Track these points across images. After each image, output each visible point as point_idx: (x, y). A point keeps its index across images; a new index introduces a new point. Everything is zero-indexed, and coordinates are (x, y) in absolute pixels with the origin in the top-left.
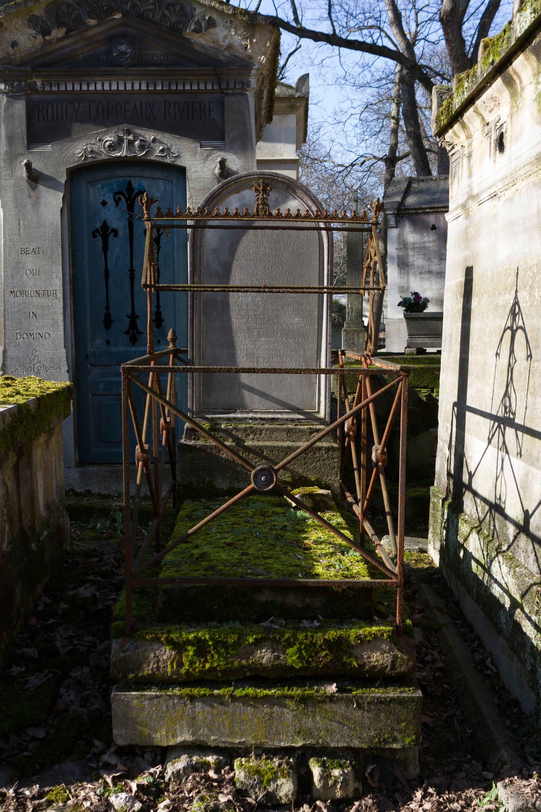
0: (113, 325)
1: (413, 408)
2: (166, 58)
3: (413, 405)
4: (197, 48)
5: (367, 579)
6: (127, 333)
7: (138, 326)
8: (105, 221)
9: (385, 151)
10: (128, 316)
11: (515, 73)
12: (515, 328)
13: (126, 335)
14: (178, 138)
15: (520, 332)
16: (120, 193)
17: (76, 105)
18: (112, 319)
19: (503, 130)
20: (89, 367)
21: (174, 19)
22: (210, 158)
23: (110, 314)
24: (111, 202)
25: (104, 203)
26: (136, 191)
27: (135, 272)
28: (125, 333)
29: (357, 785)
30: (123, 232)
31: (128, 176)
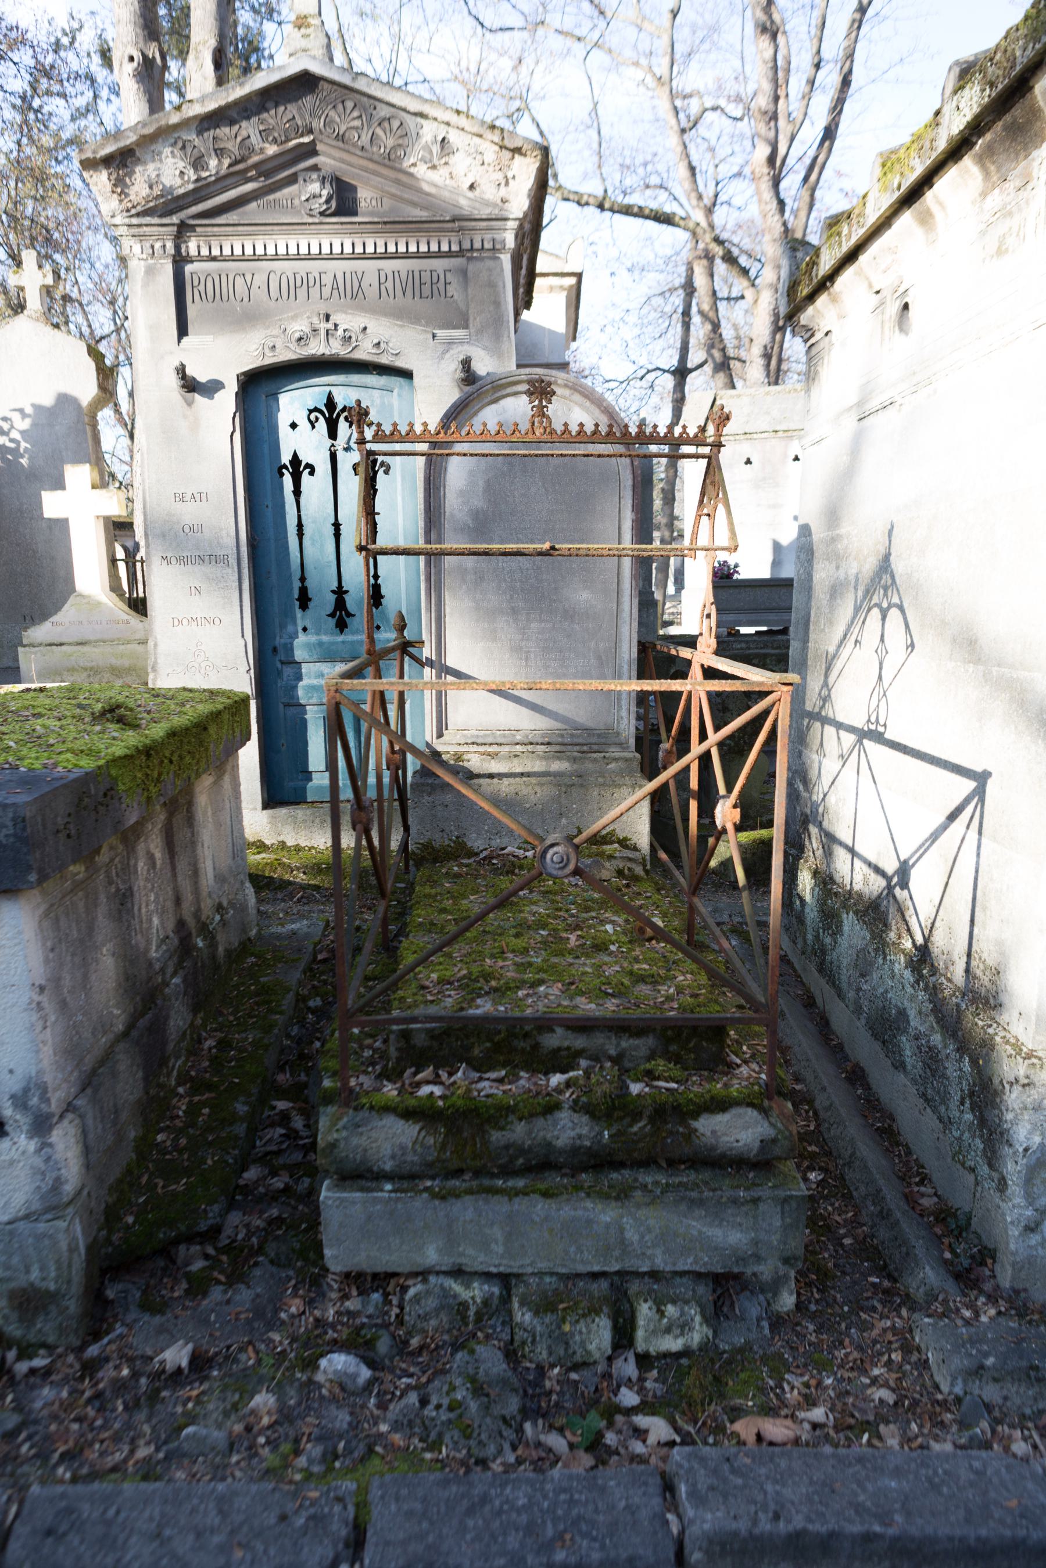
0: (311, 604)
4: (426, 188)
6: (332, 615)
9: (671, 360)
10: (333, 592)
11: (940, 204)
12: (885, 605)
14: (401, 326)
15: (894, 613)
16: (316, 410)
17: (249, 278)
19: (906, 300)
20: (279, 665)
21: (391, 142)
22: (448, 355)
25: (294, 426)
26: (339, 407)
30: (323, 467)
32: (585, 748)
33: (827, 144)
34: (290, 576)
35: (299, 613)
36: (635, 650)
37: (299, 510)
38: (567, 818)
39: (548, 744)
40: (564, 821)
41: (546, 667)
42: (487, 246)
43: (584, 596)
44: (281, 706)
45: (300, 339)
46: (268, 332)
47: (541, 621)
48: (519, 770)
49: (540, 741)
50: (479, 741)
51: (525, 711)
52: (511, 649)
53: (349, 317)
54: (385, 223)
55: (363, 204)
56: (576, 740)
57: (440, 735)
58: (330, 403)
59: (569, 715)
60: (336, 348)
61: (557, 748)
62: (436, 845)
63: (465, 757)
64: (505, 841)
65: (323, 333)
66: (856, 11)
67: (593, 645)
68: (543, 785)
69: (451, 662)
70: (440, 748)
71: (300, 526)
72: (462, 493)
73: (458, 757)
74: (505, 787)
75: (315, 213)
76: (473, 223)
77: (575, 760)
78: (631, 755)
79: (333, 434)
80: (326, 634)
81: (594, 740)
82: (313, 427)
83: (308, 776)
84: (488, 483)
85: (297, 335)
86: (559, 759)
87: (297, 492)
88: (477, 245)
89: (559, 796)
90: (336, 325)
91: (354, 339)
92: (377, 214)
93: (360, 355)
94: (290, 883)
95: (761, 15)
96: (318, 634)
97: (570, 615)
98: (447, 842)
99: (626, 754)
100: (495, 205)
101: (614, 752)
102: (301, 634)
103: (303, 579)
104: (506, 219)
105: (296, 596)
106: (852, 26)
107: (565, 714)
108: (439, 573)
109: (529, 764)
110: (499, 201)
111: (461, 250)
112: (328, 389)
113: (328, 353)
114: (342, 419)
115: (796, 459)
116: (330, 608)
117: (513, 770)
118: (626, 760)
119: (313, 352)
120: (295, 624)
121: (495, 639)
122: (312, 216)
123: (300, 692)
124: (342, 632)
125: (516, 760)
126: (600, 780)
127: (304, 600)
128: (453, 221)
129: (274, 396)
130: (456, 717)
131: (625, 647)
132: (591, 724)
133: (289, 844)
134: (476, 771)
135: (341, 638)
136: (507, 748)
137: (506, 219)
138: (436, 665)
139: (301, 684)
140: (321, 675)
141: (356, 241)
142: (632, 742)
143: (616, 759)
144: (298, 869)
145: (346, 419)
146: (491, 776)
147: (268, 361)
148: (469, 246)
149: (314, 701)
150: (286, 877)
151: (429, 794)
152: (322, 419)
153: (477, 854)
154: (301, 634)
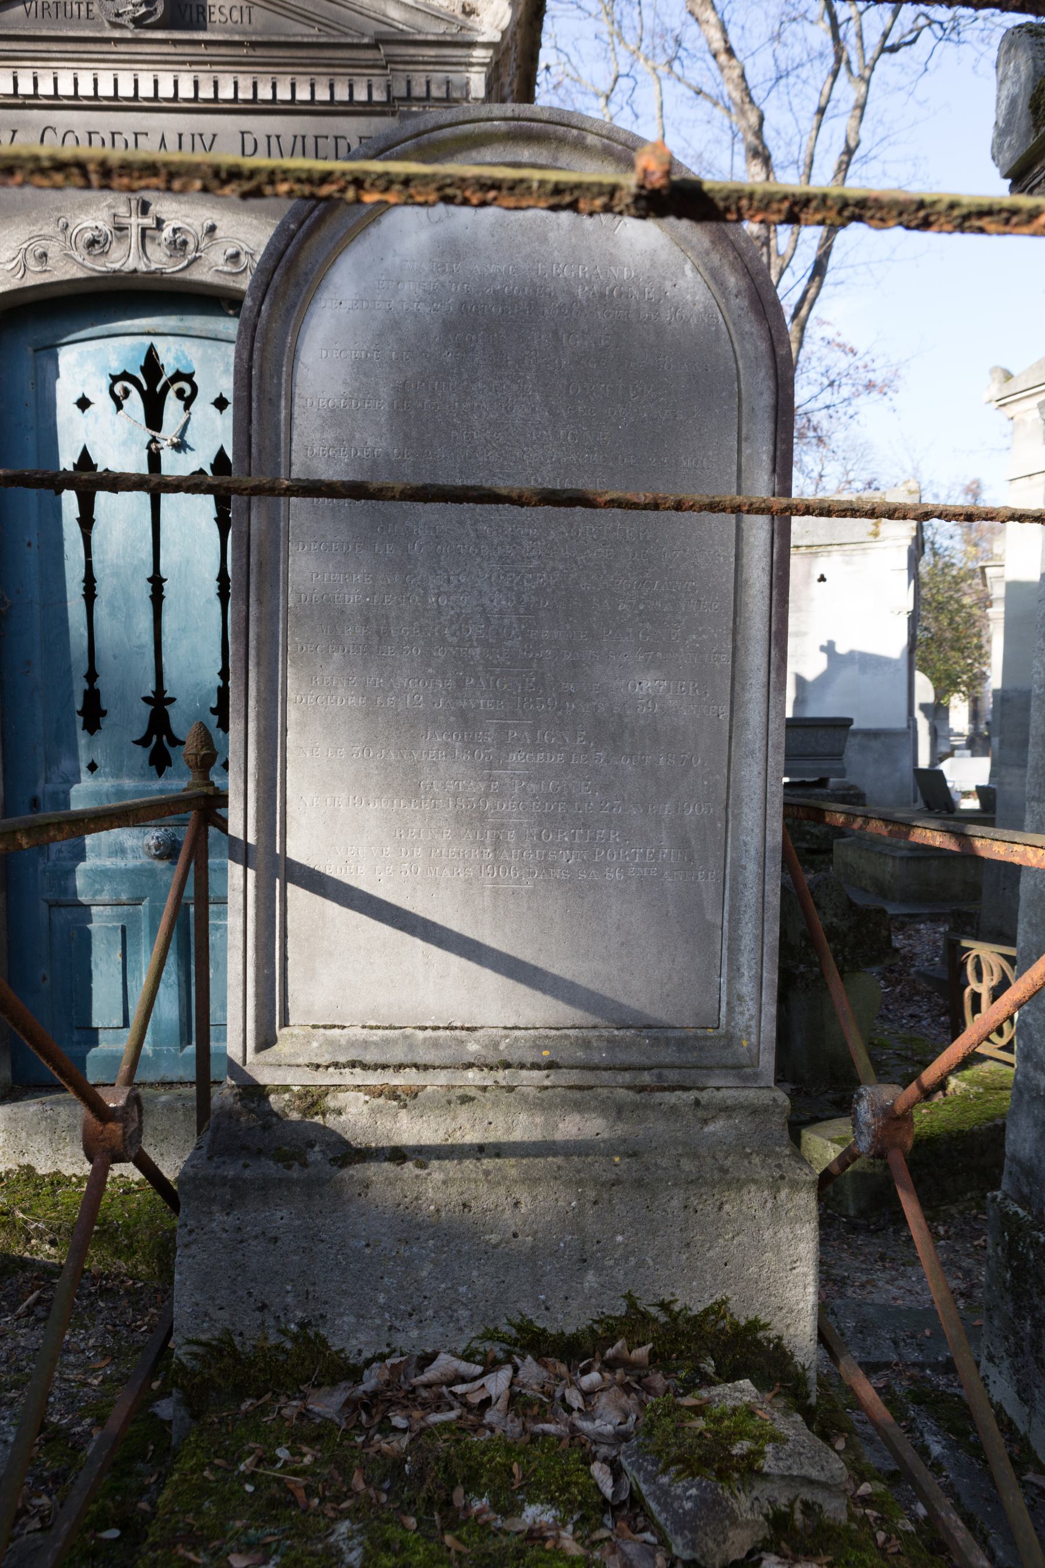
0: (105, 722)
1: (834, 920)
2: (246, 19)
3: (836, 915)
5: (1015, 135)
7: (174, 725)
8: (85, 448)
13: (139, 748)
16: (125, 376)
18: (104, 707)
23: (98, 691)
24: (102, 401)
25: (84, 403)
26: (168, 373)
27: (165, 585)
28: (136, 742)
29: (832, 945)
31: (148, 334)
32: (646, 1078)
33: (817, 279)
34: (69, 670)
35: (83, 738)
36: (776, 825)
37: (88, 553)
38: (600, 1270)
39: (551, 1065)
40: (591, 1279)
41: (548, 866)
42: (436, 93)
43: (647, 684)
44: (44, 907)
45: (92, 243)
46: (35, 230)
47: (536, 747)
48: (472, 1137)
49: (529, 1058)
50: (369, 1058)
51: (489, 979)
52: (457, 817)
53: (184, 209)
54: (254, 45)
55: (216, 17)
56: (623, 1057)
57: (266, 1041)
58: (152, 365)
59: (605, 990)
60: (158, 260)
61: (574, 1077)
62: (246, 1346)
63: (330, 1102)
64: (431, 1337)
65: (134, 233)
66: (843, 153)
67: (667, 809)
68: (536, 1181)
69: (301, 847)
70: (265, 1077)
71: (89, 580)
72: (334, 417)
73: (313, 1100)
74: (435, 1188)
75: (125, 20)
76: (412, 51)
77: (619, 1111)
78: (764, 1097)
79: (154, 419)
80: (131, 775)
81: (667, 1055)
82: (119, 407)
83: (91, 1036)
84: (403, 393)
85: (88, 235)
86: (579, 1107)
87: (86, 521)
88: (419, 91)
89: (581, 1211)
90: (160, 222)
91: (191, 246)
92: (244, 33)
93: (202, 274)
94: (24, 1264)
95: (751, 138)
96: (117, 774)
97: (612, 732)
98: (273, 1340)
99: (750, 1095)
100: (449, 20)
101: (723, 1089)
102: (85, 777)
103: (92, 675)
104: (471, 45)
105: (79, 707)
106: (839, 167)
107: (595, 986)
108: (270, 618)
109: (500, 1122)
110: (458, 12)
111: (391, 100)
112: (147, 340)
113: (142, 267)
114: (171, 394)
115: (822, 579)
116: (140, 729)
117: (458, 1139)
118: (754, 1111)
119: (117, 266)
120: (75, 757)
121: (414, 792)
122: (115, 25)
123: (80, 882)
124: (160, 772)
125: (464, 1114)
126: (687, 1165)
127: (93, 714)
128: (375, 46)
129: (50, 350)
130: (309, 994)
131: (750, 816)
132: (659, 1013)
133: (41, 1171)
134: (358, 1139)
135: (157, 784)
136: (442, 1078)
137: (471, 45)
138: (260, 857)
139: (82, 866)
140: (120, 851)
141: (202, 77)
142: (767, 1061)
143: (727, 1110)
144: (40, 1234)
145: (180, 394)
146: (398, 1155)
147: (31, 281)
148: (403, 93)
149: (105, 897)
150: (17, 1250)
151: (229, 1208)
152: (135, 393)
153: (355, 1374)
154: (85, 777)
